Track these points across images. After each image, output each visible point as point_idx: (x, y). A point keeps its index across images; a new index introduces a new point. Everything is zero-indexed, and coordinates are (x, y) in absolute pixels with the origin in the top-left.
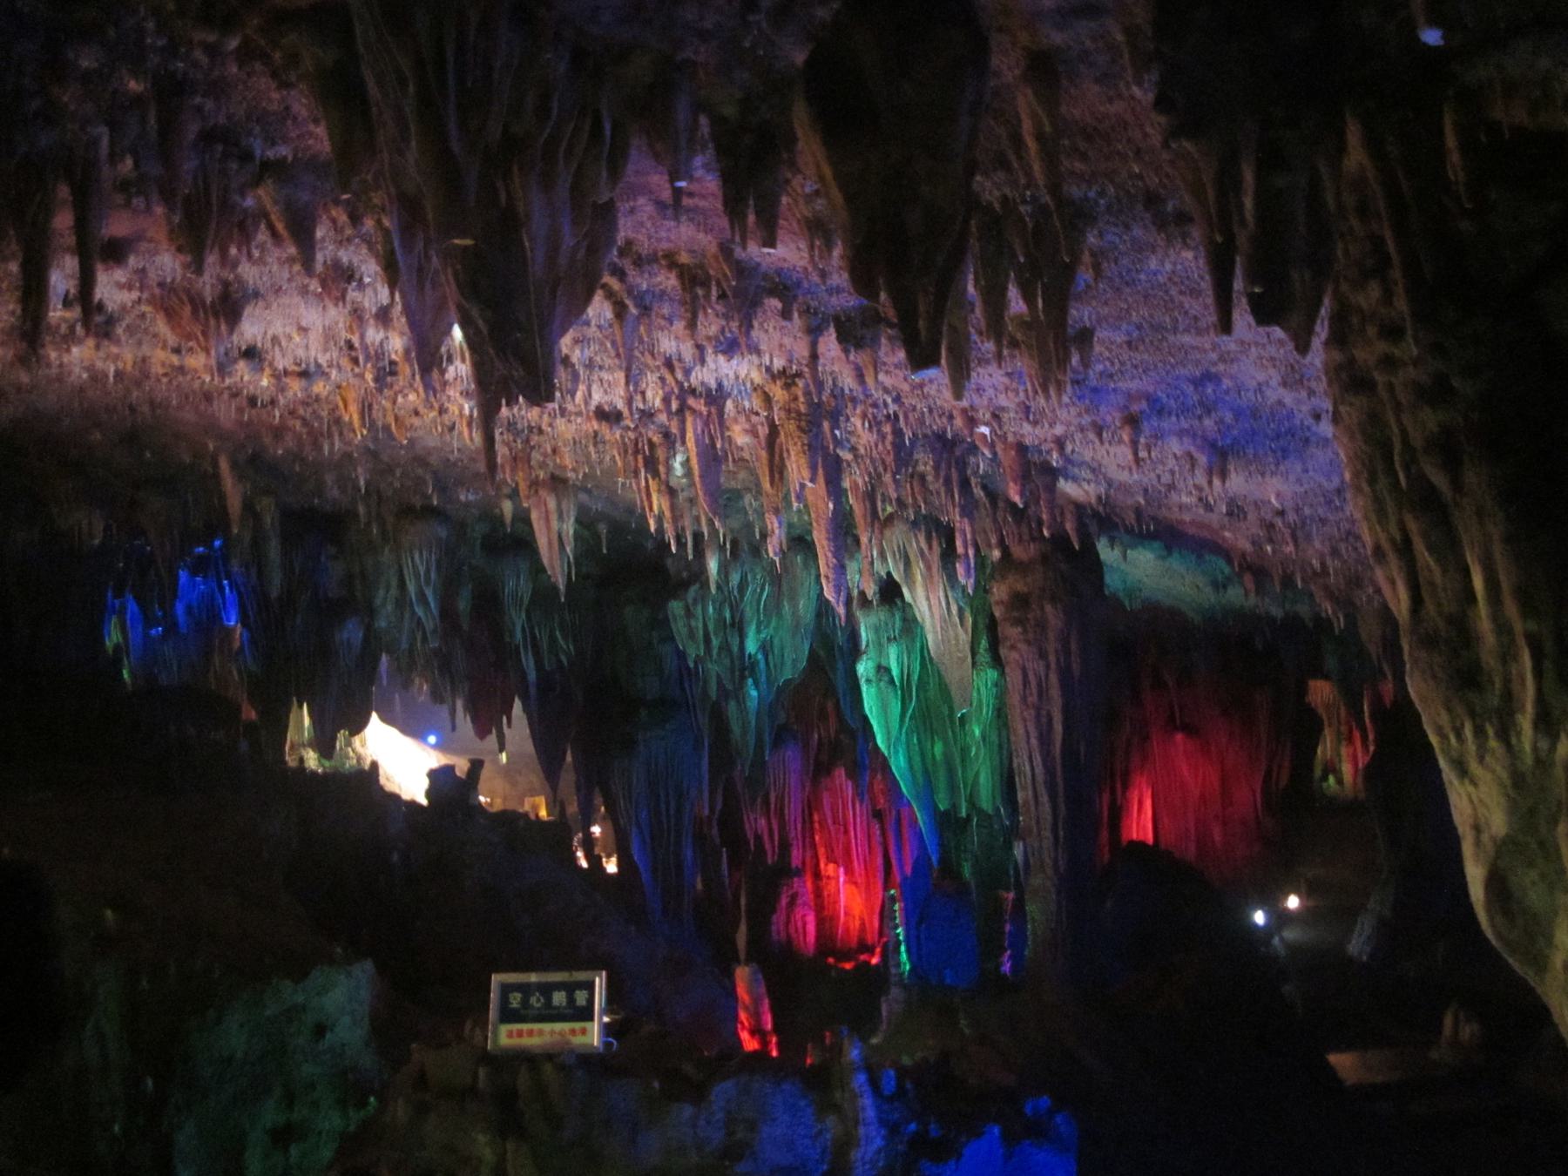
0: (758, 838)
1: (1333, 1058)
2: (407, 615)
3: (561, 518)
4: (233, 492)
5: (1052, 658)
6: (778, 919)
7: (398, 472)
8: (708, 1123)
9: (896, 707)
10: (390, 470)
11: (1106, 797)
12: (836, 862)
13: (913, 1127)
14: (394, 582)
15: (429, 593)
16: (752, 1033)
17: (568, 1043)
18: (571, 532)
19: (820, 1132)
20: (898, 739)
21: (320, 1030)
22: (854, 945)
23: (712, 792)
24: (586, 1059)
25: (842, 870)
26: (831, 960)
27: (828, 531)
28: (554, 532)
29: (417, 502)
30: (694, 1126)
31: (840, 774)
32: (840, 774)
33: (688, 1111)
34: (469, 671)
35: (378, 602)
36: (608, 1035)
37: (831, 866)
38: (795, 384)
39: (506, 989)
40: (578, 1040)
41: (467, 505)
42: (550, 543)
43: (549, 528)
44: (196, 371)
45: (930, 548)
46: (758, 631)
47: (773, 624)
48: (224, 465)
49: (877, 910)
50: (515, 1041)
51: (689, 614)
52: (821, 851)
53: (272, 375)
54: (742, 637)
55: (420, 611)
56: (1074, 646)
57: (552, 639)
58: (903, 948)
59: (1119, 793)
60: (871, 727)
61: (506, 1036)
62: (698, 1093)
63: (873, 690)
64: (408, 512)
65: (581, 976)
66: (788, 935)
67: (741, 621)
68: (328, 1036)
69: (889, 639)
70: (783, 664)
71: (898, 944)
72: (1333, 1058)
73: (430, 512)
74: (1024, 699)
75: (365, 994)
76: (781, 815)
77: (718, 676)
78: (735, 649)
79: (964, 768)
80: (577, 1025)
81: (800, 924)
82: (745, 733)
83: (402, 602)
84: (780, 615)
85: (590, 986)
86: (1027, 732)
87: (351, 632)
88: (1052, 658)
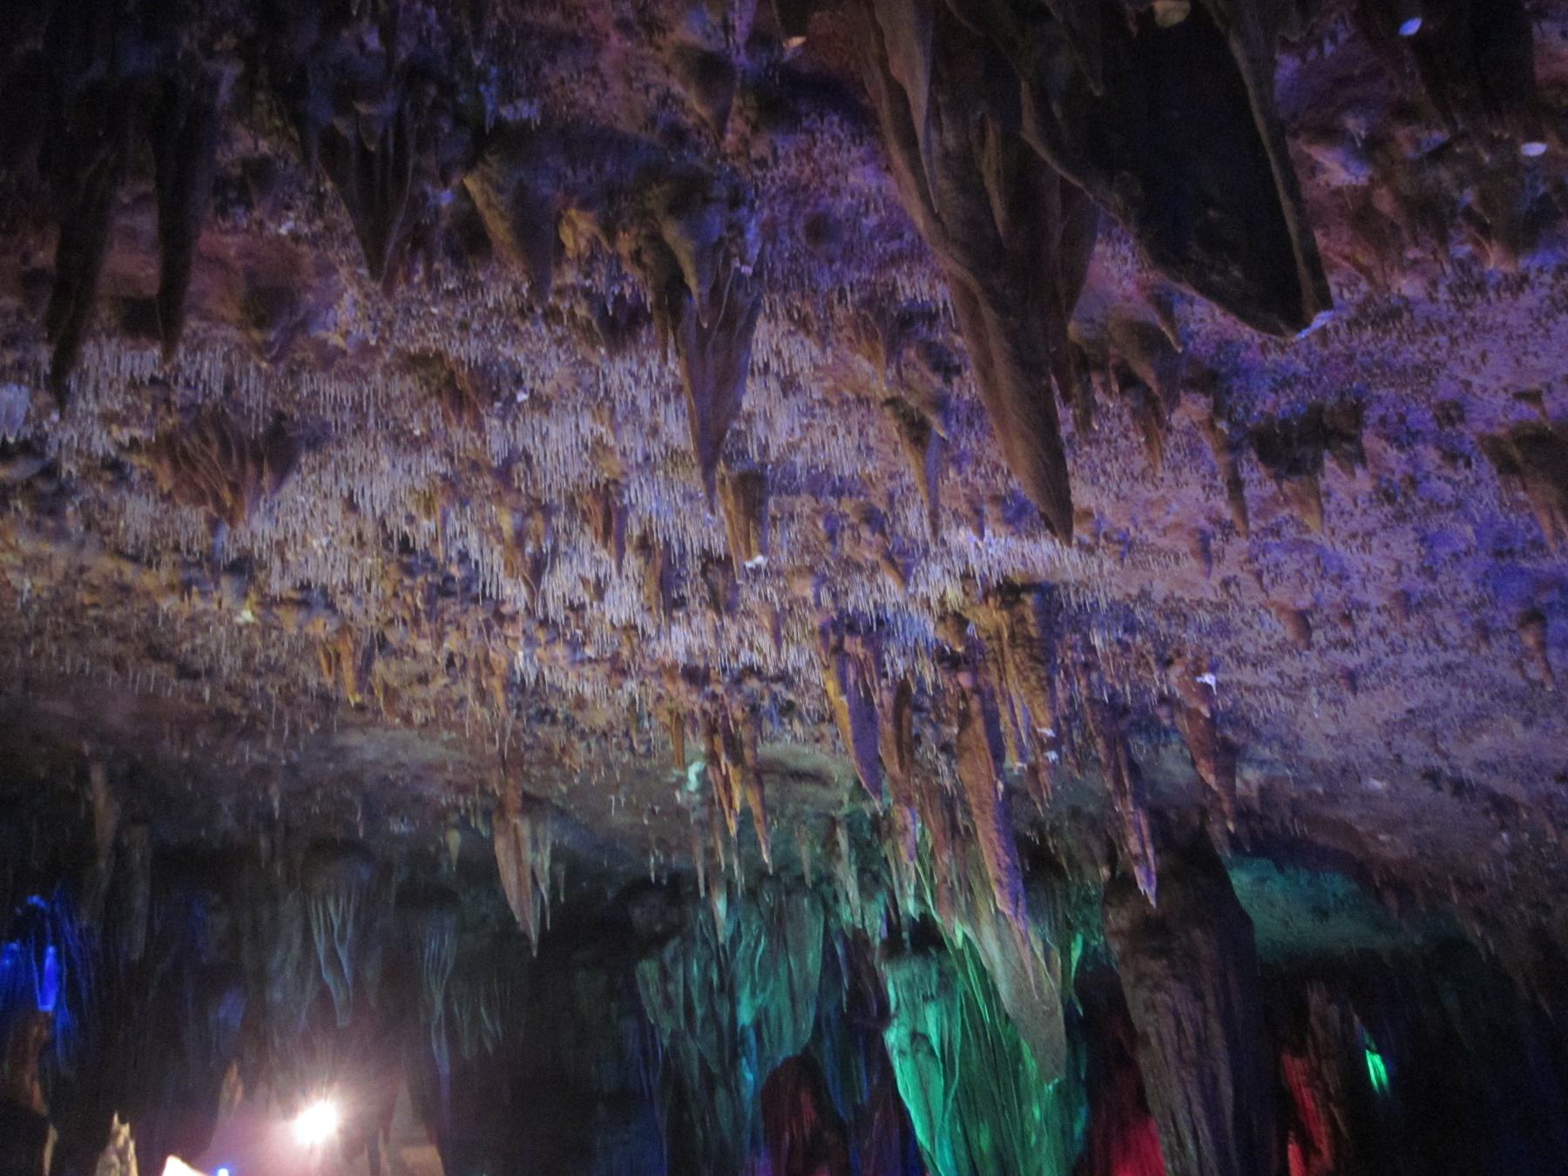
7: (319, 793)
9: (938, 1083)
10: (308, 792)
18: (547, 865)
27: (995, 819)
29: (339, 833)
35: (275, 962)
41: (399, 839)
43: (519, 862)
44: (147, 594)
46: (753, 995)
48: (97, 776)
51: (665, 976)
54: (734, 1003)
55: (328, 977)
60: (908, 1112)
63: (908, 1065)
69: (926, 999)
70: (781, 1038)
73: (350, 848)
74: (1179, 1053)
77: (702, 1060)
78: (725, 1020)
79: (1025, 1161)
84: (776, 974)
86: (1188, 1098)
88: (1210, 1001)
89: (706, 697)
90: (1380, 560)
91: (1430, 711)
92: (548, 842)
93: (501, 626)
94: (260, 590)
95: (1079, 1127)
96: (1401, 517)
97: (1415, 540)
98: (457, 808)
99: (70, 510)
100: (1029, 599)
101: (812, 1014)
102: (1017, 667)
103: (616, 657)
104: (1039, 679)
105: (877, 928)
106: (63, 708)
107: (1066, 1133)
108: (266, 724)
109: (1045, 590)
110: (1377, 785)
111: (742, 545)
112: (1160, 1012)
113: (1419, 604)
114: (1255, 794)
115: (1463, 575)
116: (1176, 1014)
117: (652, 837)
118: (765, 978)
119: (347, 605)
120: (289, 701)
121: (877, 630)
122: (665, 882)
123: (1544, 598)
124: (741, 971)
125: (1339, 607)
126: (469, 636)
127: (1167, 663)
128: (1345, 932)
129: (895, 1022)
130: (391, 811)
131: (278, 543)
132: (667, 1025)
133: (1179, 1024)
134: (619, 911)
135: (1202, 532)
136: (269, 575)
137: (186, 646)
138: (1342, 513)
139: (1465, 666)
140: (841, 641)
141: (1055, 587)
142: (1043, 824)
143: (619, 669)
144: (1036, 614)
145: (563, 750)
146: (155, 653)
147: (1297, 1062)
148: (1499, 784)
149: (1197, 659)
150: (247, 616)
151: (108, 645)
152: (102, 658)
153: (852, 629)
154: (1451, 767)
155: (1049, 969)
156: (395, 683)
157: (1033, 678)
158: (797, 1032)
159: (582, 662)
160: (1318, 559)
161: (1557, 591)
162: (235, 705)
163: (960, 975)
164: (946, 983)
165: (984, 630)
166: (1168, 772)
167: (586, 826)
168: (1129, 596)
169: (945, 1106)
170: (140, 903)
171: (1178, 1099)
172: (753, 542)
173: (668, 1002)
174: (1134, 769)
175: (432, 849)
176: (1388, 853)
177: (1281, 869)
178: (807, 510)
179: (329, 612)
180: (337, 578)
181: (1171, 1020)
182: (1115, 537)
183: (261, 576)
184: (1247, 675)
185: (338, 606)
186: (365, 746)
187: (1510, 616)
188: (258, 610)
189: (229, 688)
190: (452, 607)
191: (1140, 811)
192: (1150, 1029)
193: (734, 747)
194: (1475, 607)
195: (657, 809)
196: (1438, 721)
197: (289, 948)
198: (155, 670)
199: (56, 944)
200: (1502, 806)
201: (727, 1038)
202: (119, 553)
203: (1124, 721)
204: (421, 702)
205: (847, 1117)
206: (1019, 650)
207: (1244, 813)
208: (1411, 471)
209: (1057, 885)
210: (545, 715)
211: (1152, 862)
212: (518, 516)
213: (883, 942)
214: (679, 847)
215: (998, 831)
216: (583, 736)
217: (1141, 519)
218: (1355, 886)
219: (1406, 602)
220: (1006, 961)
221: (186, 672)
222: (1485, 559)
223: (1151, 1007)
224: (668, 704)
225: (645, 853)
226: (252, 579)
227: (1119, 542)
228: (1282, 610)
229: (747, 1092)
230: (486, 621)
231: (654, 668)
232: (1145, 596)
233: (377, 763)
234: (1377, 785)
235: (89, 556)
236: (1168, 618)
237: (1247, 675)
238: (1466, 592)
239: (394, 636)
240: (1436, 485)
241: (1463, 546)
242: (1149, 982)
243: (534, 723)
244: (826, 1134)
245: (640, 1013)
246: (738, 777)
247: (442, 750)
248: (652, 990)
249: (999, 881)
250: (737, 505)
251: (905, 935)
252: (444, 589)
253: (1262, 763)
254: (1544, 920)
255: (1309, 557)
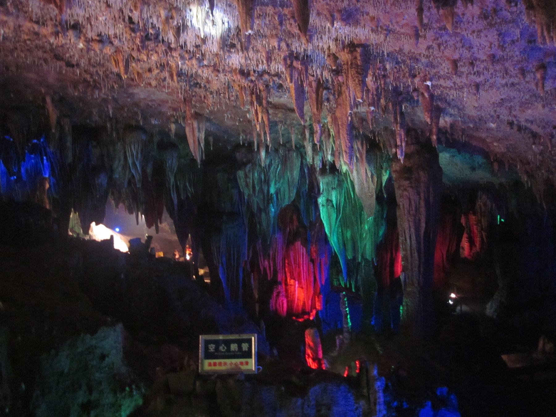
0: (265, 269)
1: (504, 357)
2: (127, 173)
3: (199, 131)
4: (53, 114)
5: (422, 195)
6: (272, 302)
8: (308, 406)
9: (334, 216)
10: (122, 108)
11: (389, 255)
12: (294, 279)
13: (395, 404)
14: (122, 158)
15: (137, 164)
16: (314, 360)
17: (240, 368)
18: (203, 137)
19: (357, 409)
20: (334, 230)
21: (103, 357)
22: (300, 312)
23: (249, 250)
24: (249, 377)
25: (297, 282)
26: (294, 318)
28: (196, 137)
29: (134, 123)
30: (303, 408)
31: (298, 244)
32: (298, 244)
33: (300, 401)
34: (150, 198)
36: (258, 366)
37: (292, 281)
38: (355, 51)
39: (207, 343)
40: (244, 367)
41: (155, 126)
42: (194, 141)
43: (194, 135)
44: (45, 36)
45: (362, 148)
46: (275, 184)
47: (282, 181)
48: (48, 100)
49: (311, 298)
50: (213, 368)
51: (246, 176)
52: (288, 275)
53: (86, 41)
54: (269, 186)
55: (133, 171)
56: (431, 189)
57: (185, 186)
58: (349, 317)
59: (394, 254)
61: (207, 366)
62: (302, 391)
63: (325, 209)
64: (132, 128)
65: (245, 336)
66: (276, 308)
67: (268, 180)
68: (107, 359)
69: (333, 189)
70: (284, 198)
71: (347, 314)
72: (504, 357)
73: (139, 128)
74: (409, 212)
75: (120, 339)
76: (274, 260)
77: (258, 204)
78: (266, 191)
80: (243, 360)
81: (281, 304)
82: (268, 225)
83: (125, 166)
84: (284, 179)
85: (250, 341)
87: (102, 180)
88: (422, 195)
89: (249, 81)
90: (484, 42)
91: (510, 100)
92: (204, 129)
93: (171, 53)
94: (85, 35)
95: (381, 233)
96: (491, 25)
97: (497, 35)
98: (174, 116)
99: (9, 4)
100: (359, 50)
101: (295, 191)
102: (352, 76)
103: (215, 65)
104: (359, 81)
105: (318, 164)
106: (32, 76)
107: (376, 234)
108: (100, 84)
109: (365, 46)
110: (493, 125)
111: (244, 26)
112: (405, 198)
113: (498, 60)
114: (448, 126)
115: (516, 49)
116: (409, 199)
117: (241, 129)
118: (280, 180)
119: (116, 42)
120: (107, 76)
121: (306, 60)
122: (246, 145)
123: (547, 60)
124: (272, 176)
125: (468, 59)
126: (160, 56)
127: (414, 76)
128: (482, 176)
129: (322, 196)
130: (152, 116)
131: (87, 18)
132: (246, 192)
133: (410, 202)
134: (228, 155)
135: (416, 27)
136: (87, 31)
137: (67, 55)
138: (469, 22)
139: (518, 84)
140: (292, 63)
141: (369, 46)
142: (375, 132)
143: (216, 69)
144: (361, 56)
145: (205, 97)
146: (58, 57)
147: (474, 217)
148: (534, 128)
149: (426, 76)
150: (81, 45)
151: (40, 54)
152: (39, 59)
153: (297, 58)
154: (517, 120)
155: (372, 181)
156: (140, 71)
157: (357, 80)
158: (289, 197)
159: (203, 66)
160: (461, 40)
161: (553, 57)
162: (88, 77)
163: (345, 182)
164: (340, 184)
165: (343, 61)
166: (419, 116)
167: (218, 124)
168: (396, 50)
169: (336, 223)
170: (69, 144)
171: (406, 225)
172: (248, 25)
173: (247, 185)
174: (402, 114)
175: (167, 130)
176: (497, 150)
177: (459, 152)
178: (271, 12)
179: (110, 45)
180: (111, 33)
181: (407, 201)
182: (385, 28)
183: (84, 31)
184: (442, 82)
185: (114, 42)
186: (140, 93)
187: (533, 66)
188: (85, 44)
189: (85, 71)
190: (151, 44)
191: (402, 130)
192: (401, 203)
193: (259, 99)
194: (519, 62)
195: (241, 120)
196: (512, 104)
197: (120, 161)
198: (59, 63)
199: (46, 155)
200: (535, 135)
201: (266, 197)
202: (31, 20)
203: (399, 96)
204: (152, 78)
205: (307, 224)
206: (353, 69)
207: (440, 131)
208: (495, 6)
209: (378, 153)
210: (197, 84)
211: (404, 148)
212: (166, 11)
213: (320, 169)
214: (250, 133)
215: (347, 134)
216: (211, 93)
217: (394, 21)
218: (485, 161)
219: (493, 58)
220: (358, 178)
221: (69, 64)
222: (523, 43)
223: (402, 196)
224: (238, 83)
225: (239, 134)
226: (81, 32)
227: (386, 30)
228: (448, 59)
229: (272, 215)
230: (165, 50)
231: (230, 70)
232: (401, 50)
233: (144, 99)
234: (493, 125)
235: (21, 21)
236: (410, 59)
237: (442, 82)
238: (517, 56)
239: (135, 54)
240: (504, 13)
241: (516, 38)
242: (402, 188)
243: (193, 88)
244: (300, 229)
245: (237, 186)
246: (261, 111)
247: (167, 96)
248: (242, 180)
249: (346, 151)
250: (243, 9)
251: (327, 167)
252: (147, 38)
253: (451, 115)
254: (550, 176)
255: (458, 39)
